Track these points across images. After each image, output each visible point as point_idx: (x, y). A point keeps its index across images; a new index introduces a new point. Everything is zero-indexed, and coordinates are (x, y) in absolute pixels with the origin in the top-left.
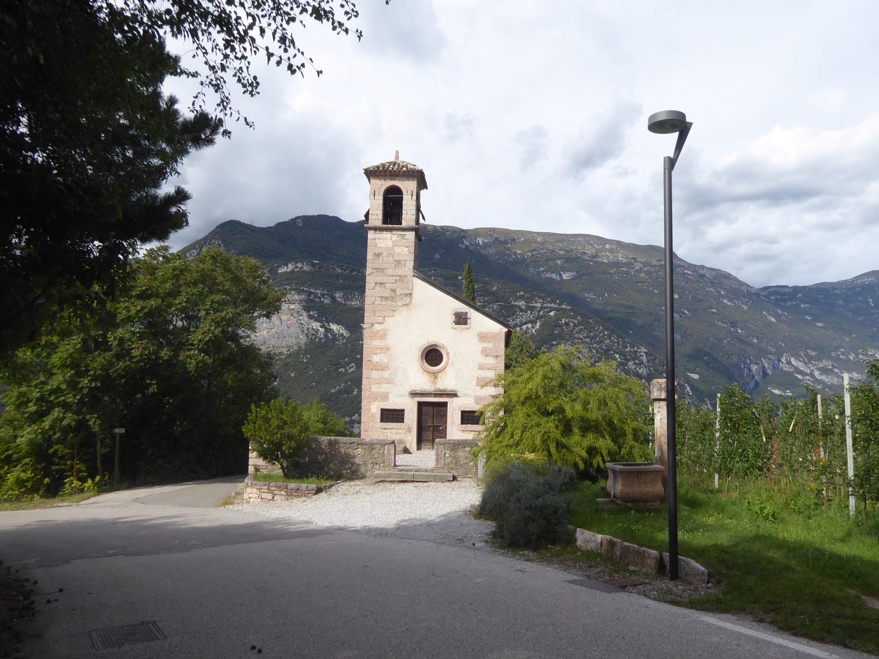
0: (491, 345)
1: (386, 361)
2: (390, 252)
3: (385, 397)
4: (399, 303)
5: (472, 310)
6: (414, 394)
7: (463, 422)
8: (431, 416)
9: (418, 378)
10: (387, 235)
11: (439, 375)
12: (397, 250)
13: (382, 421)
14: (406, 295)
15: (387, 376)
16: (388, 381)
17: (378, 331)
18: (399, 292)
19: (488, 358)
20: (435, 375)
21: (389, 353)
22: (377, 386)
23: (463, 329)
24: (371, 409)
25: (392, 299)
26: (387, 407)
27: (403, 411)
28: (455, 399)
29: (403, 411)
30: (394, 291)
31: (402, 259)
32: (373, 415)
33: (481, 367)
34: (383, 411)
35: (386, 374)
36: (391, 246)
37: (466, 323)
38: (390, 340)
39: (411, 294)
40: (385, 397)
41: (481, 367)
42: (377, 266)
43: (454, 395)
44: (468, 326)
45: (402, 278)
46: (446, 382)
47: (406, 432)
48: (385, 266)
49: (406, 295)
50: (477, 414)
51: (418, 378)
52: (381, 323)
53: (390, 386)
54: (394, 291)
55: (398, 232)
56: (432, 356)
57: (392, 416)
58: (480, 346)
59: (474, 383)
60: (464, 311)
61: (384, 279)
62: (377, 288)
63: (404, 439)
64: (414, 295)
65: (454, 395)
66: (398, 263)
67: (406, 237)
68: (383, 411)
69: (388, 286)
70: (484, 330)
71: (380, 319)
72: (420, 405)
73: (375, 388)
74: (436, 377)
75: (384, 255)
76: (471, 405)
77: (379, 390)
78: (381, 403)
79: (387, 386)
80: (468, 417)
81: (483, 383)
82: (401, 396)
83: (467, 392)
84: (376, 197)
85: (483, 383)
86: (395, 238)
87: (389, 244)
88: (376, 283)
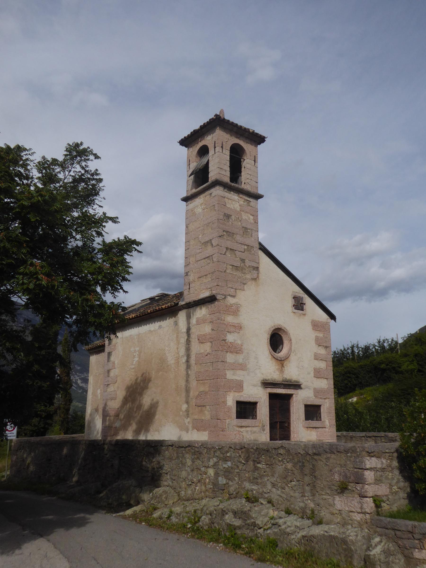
1: (239, 342)
4: (248, 276)
6: (266, 384)
9: (264, 366)
15: (241, 361)
16: (242, 367)
17: (231, 305)
19: (320, 347)
20: (281, 362)
21: (241, 332)
26: (242, 399)
27: (255, 404)
28: (300, 392)
29: (255, 404)
32: (229, 408)
34: (239, 403)
35: (240, 358)
51: (264, 366)
55: (245, 197)
59: (312, 374)
61: (235, 246)
65: (297, 386)
68: (239, 403)
70: (316, 318)
72: (272, 396)
74: (283, 366)
80: (312, 412)
87: (237, 206)
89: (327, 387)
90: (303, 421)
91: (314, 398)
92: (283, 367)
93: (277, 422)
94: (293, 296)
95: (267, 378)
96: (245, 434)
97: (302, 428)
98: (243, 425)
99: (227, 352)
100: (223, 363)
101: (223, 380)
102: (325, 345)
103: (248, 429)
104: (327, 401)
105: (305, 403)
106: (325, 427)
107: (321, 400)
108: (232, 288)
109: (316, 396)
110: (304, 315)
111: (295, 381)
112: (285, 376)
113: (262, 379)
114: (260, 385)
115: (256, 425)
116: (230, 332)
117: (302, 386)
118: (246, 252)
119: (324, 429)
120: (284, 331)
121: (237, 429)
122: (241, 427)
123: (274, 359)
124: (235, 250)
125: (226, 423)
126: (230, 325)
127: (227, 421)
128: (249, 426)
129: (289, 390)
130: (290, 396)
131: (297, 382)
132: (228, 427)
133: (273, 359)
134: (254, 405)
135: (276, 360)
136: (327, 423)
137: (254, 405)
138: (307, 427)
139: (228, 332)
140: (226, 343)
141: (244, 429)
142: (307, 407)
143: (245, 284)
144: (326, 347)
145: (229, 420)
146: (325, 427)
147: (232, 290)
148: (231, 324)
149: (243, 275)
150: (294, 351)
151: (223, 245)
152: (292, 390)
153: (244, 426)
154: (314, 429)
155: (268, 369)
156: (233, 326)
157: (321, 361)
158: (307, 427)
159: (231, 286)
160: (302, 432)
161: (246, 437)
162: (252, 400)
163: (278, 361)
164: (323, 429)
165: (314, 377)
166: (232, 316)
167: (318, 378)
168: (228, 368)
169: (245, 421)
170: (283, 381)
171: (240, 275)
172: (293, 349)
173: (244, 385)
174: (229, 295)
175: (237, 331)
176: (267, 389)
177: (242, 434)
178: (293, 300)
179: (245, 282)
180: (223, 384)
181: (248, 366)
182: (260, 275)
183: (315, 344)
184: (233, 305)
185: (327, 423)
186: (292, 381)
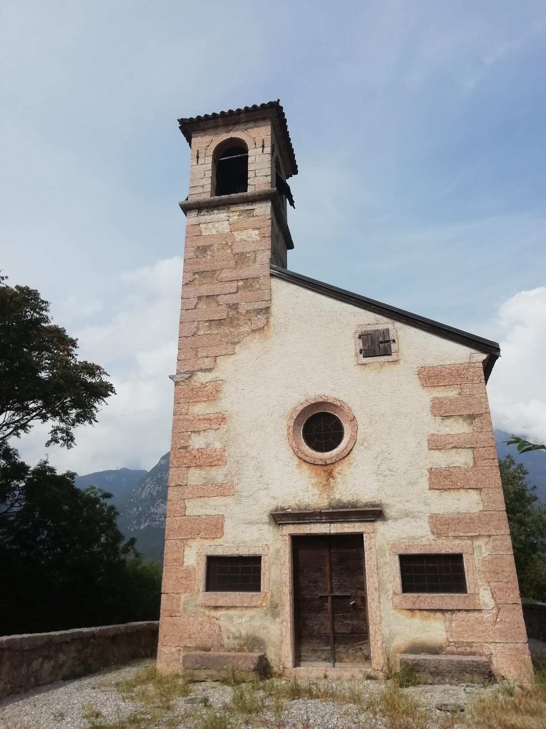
0: (452, 393)
1: (218, 445)
2: (227, 242)
3: (215, 526)
4: (245, 329)
5: (398, 324)
6: (280, 518)
7: (212, 585)
8: (327, 568)
9: (288, 478)
10: (221, 215)
11: (338, 469)
12: (238, 236)
13: (210, 586)
14: (259, 311)
15: (220, 479)
16: (224, 490)
17: (204, 385)
18: (243, 308)
19: (448, 422)
20: (327, 470)
21: (224, 428)
22: (199, 501)
23: (382, 365)
24: (186, 561)
25: (231, 321)
26: (220, 552)
27: (257, 559)
28: (379, 525)
29: (257, 559)
30: (234, 307)
31: (248, 249)
32: (189, 573)
33: (436, 444)
34: (212, 562)
35: (218, 474)
36: (227, 231)
37: (387, 352)
38: (226, 403)
39: (267, 309)
40: (215, 526)
41: (436, 444)
42: (202, 267)
43: (374, 514)
44: (394, 357)
45: (248, 282)
46: (356, 483)
47: (264, 620)
48: (218, 265)
49: (259, 311)
50: (209, 387)
51: (288, 478)
52: (209, 370)
53: (228, 500)
54: (234, 307)
55: (241, 208)
56: (321, 428)
57: (234, 573)
58: (426, 397)
59: (425, 483)
60: (381, 327)
61: (216, 289)
62: (202, 306)
63: (261, 634)
64: (274, 310)
65: (374, 514)
66: (241, 258)
67: (256, 213)
68: (212, 562)
69: (223, 299)
70: (432, 362)
71: (208, 363)
72: (297, 542)
73: (195, 508)
74: (330, 475)
75: (215, 248)
76: (422, 538)
77: (202, 512)
78: (208, 543)
79: (220, 501)
80: (432, 574)
81: (443, 481)
82: (251, 523)
83: (408, 506)
84: (201, 161)
85: (443, 481)
86: (234, 217)
87: (225, 227)
88: (200, 298)
89: (481, 508)
90: (395, 594)
91: (432, 537)
92: (333, 477)
93: (327, 597)
94: (357, 335)
95: (286, 505)
96: (223, 623)
97: (394, 612)
98: (219, 604)
99: (189, 467)
100: (180, 488)
101: (178, 518)
102: (466, 412)
103: (232, 612)
104: (480, 542)
105: (402, 552)
106: (480, 610)
107: (457, 542)
108: (207, 357)
109: (438, 534)
110: (395, 362)
111: (366, 505)
112: (338, 496)
113: (272, 507)
114: (267, 519)
115: (254, 604)
116: (199, 432)
117: (388, 512)
118: (240, 292)
119: (476, 615)
120: (335, 406)
121: (207, 612)
122: (216, 608)
123: (305, 466)
124: (218, 295)
125: (179, 600)
126: (199, 419)
127: (183, 597)
128: (235, 607)
129: (346, 525)
130: (358, 538)
131: (373, 505)
132: (185, 609)
133: (304, 465)
134: (254, 562)
135: (312, 467)
136: (485, 598)
137: (254, 562)
138: (411, 610)
139: (194, 432)
140: (187, 452)
141: (221, 613)
142: (406, 560)
143: (235, 344)
144: (471, 417)
145: (186, 595)
146: (480, 610)
147: (207, 360)
148: (201, 417)
149: (232, 330)
150: (365, 440)
151: (192, 296)
152: (357, 525)
153: (222, 607)
154: (439, 615)
155: (295, 483)
156: (206, 419)
157: (454, 450)
158: (411, 610)
159: (205, 354)
160: (396, 621)
161: (228, 630)
162: (244, 552)
163: (317, 467)
164: (471, 614)
165: (430, 489)
166: (204, 404)
167: (445, 490)
168: (190, 496)
169: (226, 595)
170: (330, 506)
171: (227, 331)
172: (359, 437)
173: (226, 523)
174: (201, 370)
175: (215, 426)
176: (284, 527)
177: (217, 622)
178: (360, 341)
179: (237, 340)
180: (176, 526)
181: (238, 488)
182: (272, 319)
183: (430, 416)
184: (207, 385)
185: (485, 598)
186: (359, 505)
